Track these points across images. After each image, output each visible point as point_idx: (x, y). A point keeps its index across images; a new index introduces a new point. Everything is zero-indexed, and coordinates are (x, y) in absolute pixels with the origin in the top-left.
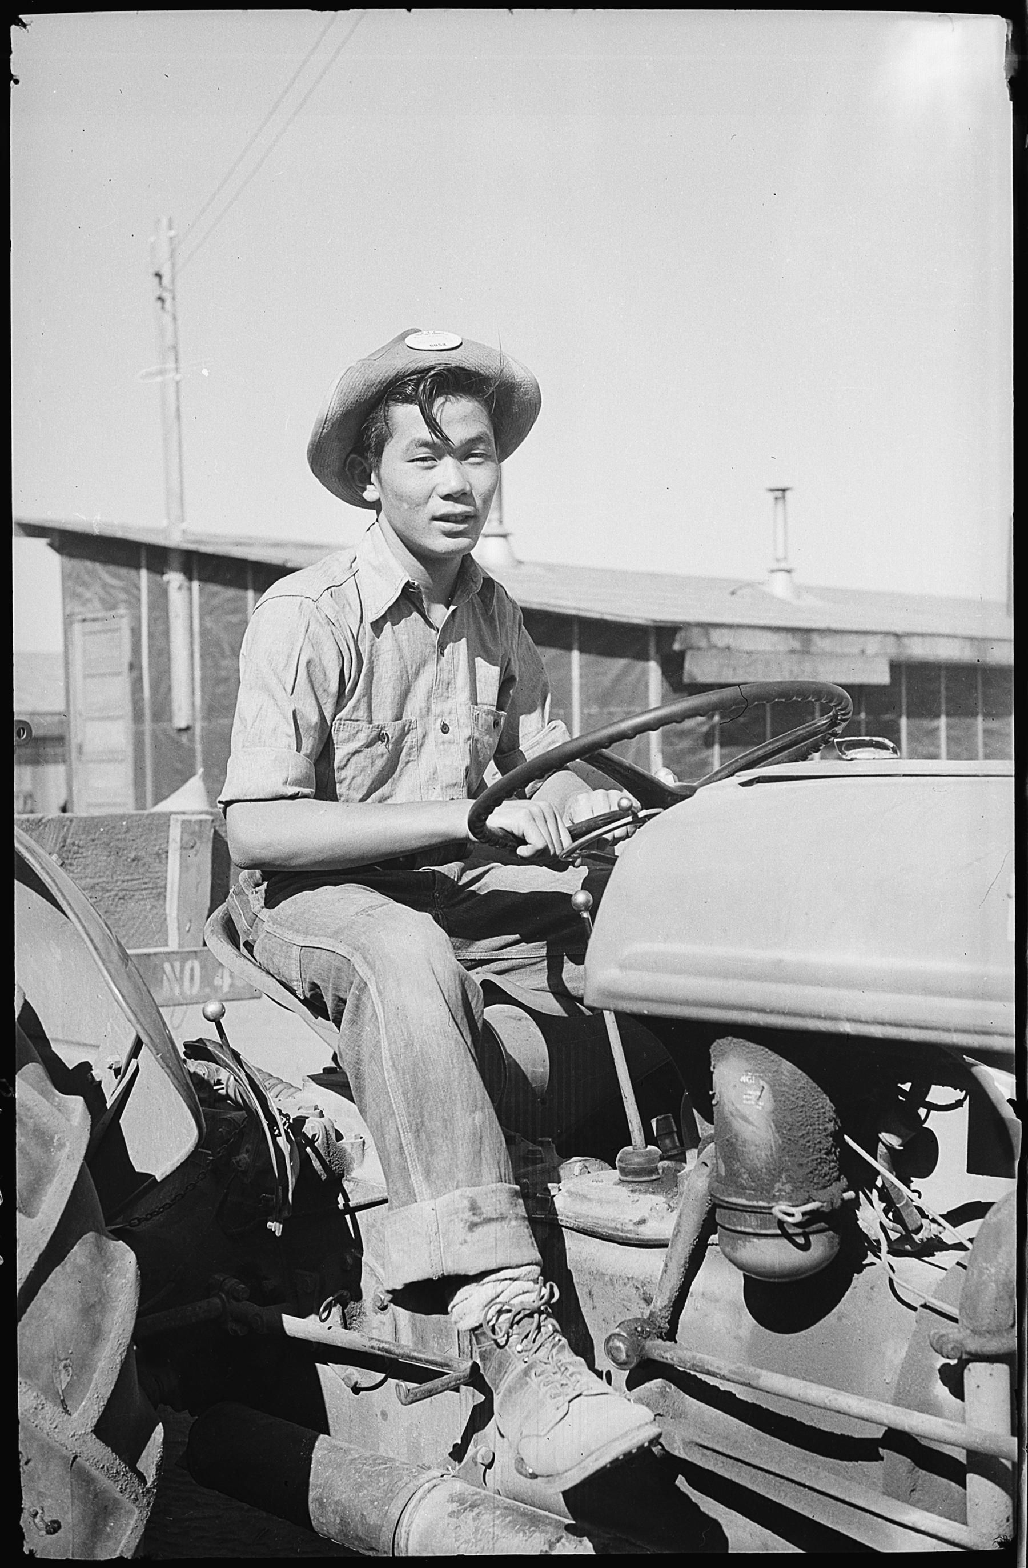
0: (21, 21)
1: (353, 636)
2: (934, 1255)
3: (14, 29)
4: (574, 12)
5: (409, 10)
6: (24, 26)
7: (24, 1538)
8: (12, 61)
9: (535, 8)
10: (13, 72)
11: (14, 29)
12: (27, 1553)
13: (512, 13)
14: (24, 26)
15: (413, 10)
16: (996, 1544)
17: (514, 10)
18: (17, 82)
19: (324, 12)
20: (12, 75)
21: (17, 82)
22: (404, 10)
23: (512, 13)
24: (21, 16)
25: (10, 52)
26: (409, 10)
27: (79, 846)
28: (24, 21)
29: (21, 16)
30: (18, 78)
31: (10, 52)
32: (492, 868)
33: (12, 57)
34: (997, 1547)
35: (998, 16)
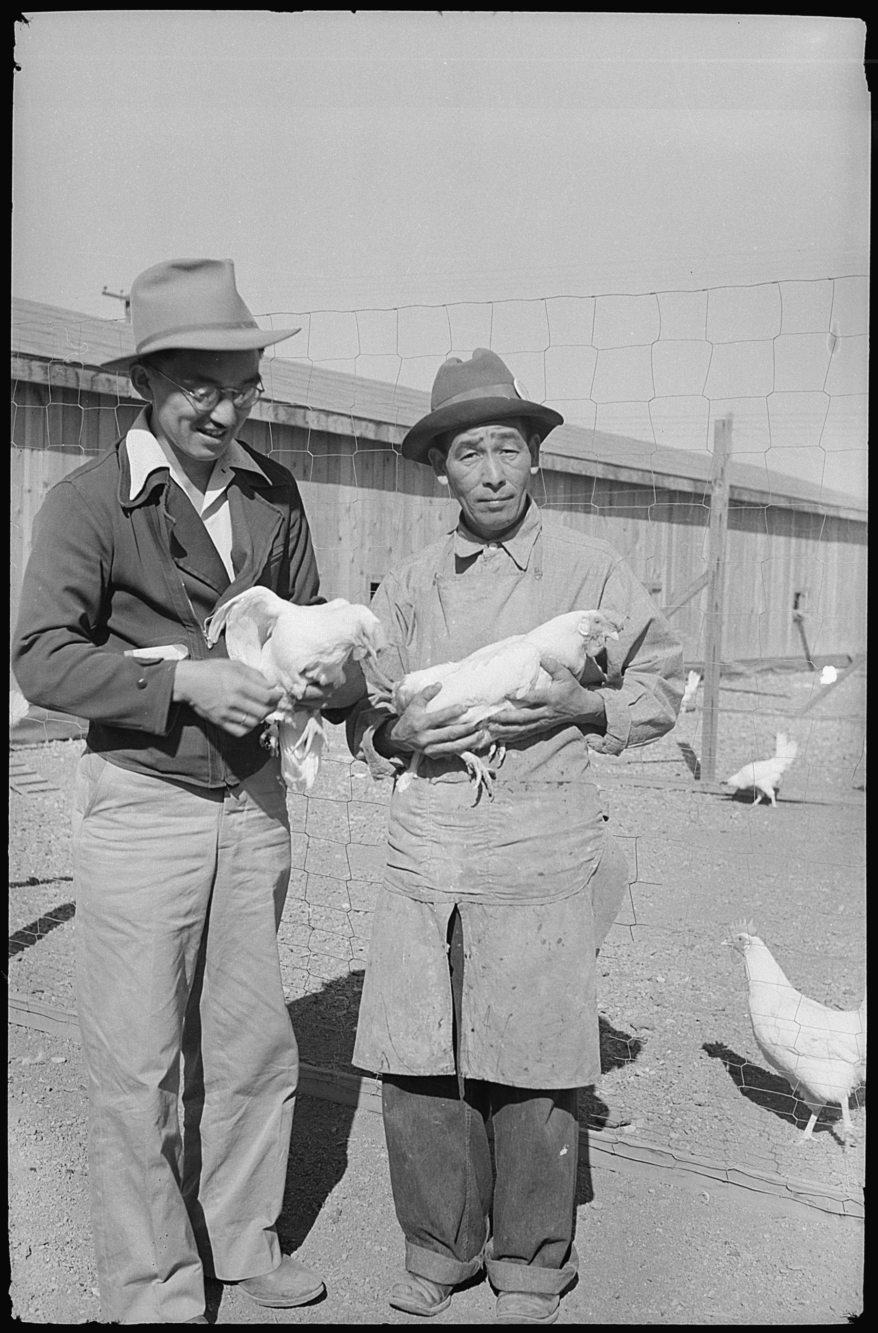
0: (23, 18)
1: (289, 525)
2: (252, 497)
3: (17, 24)
4: (494, 14)
5: (354, 12)
6: (26, 22)
7: (12, 1306)
8: (15, 51)
9: (462, 10)
10: (15, 61)
11: (17, 24)
12: (15, 1318)
13: (441, 14)
14: (26, 22)
15: (357, 12)
16: (846, 1319)
17: (443, 12)
18: (19, 69)
19: (281, 13)
20: (15, 63)
21: (19, 69)
22: (350, 12)
23: (441, 14)
24: (23, 13)
25: (13, 44)
26: (354, 12)
27: (647, 897)
28: (26, 17)
29: (23, 13)
30: (20, 66)
31: (14, 44)
32: (233, 604)
33: (15, 48)
34: (846, 1322)
35: (859, 19)
